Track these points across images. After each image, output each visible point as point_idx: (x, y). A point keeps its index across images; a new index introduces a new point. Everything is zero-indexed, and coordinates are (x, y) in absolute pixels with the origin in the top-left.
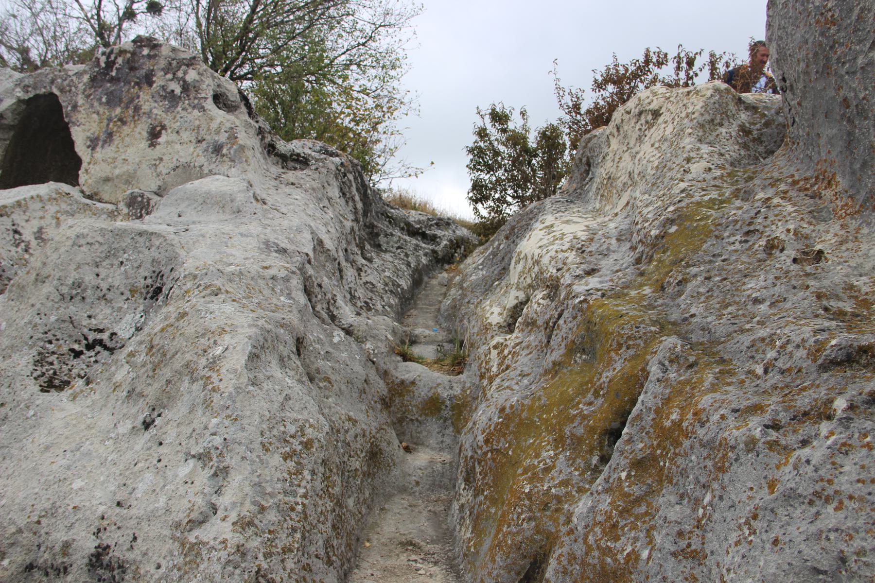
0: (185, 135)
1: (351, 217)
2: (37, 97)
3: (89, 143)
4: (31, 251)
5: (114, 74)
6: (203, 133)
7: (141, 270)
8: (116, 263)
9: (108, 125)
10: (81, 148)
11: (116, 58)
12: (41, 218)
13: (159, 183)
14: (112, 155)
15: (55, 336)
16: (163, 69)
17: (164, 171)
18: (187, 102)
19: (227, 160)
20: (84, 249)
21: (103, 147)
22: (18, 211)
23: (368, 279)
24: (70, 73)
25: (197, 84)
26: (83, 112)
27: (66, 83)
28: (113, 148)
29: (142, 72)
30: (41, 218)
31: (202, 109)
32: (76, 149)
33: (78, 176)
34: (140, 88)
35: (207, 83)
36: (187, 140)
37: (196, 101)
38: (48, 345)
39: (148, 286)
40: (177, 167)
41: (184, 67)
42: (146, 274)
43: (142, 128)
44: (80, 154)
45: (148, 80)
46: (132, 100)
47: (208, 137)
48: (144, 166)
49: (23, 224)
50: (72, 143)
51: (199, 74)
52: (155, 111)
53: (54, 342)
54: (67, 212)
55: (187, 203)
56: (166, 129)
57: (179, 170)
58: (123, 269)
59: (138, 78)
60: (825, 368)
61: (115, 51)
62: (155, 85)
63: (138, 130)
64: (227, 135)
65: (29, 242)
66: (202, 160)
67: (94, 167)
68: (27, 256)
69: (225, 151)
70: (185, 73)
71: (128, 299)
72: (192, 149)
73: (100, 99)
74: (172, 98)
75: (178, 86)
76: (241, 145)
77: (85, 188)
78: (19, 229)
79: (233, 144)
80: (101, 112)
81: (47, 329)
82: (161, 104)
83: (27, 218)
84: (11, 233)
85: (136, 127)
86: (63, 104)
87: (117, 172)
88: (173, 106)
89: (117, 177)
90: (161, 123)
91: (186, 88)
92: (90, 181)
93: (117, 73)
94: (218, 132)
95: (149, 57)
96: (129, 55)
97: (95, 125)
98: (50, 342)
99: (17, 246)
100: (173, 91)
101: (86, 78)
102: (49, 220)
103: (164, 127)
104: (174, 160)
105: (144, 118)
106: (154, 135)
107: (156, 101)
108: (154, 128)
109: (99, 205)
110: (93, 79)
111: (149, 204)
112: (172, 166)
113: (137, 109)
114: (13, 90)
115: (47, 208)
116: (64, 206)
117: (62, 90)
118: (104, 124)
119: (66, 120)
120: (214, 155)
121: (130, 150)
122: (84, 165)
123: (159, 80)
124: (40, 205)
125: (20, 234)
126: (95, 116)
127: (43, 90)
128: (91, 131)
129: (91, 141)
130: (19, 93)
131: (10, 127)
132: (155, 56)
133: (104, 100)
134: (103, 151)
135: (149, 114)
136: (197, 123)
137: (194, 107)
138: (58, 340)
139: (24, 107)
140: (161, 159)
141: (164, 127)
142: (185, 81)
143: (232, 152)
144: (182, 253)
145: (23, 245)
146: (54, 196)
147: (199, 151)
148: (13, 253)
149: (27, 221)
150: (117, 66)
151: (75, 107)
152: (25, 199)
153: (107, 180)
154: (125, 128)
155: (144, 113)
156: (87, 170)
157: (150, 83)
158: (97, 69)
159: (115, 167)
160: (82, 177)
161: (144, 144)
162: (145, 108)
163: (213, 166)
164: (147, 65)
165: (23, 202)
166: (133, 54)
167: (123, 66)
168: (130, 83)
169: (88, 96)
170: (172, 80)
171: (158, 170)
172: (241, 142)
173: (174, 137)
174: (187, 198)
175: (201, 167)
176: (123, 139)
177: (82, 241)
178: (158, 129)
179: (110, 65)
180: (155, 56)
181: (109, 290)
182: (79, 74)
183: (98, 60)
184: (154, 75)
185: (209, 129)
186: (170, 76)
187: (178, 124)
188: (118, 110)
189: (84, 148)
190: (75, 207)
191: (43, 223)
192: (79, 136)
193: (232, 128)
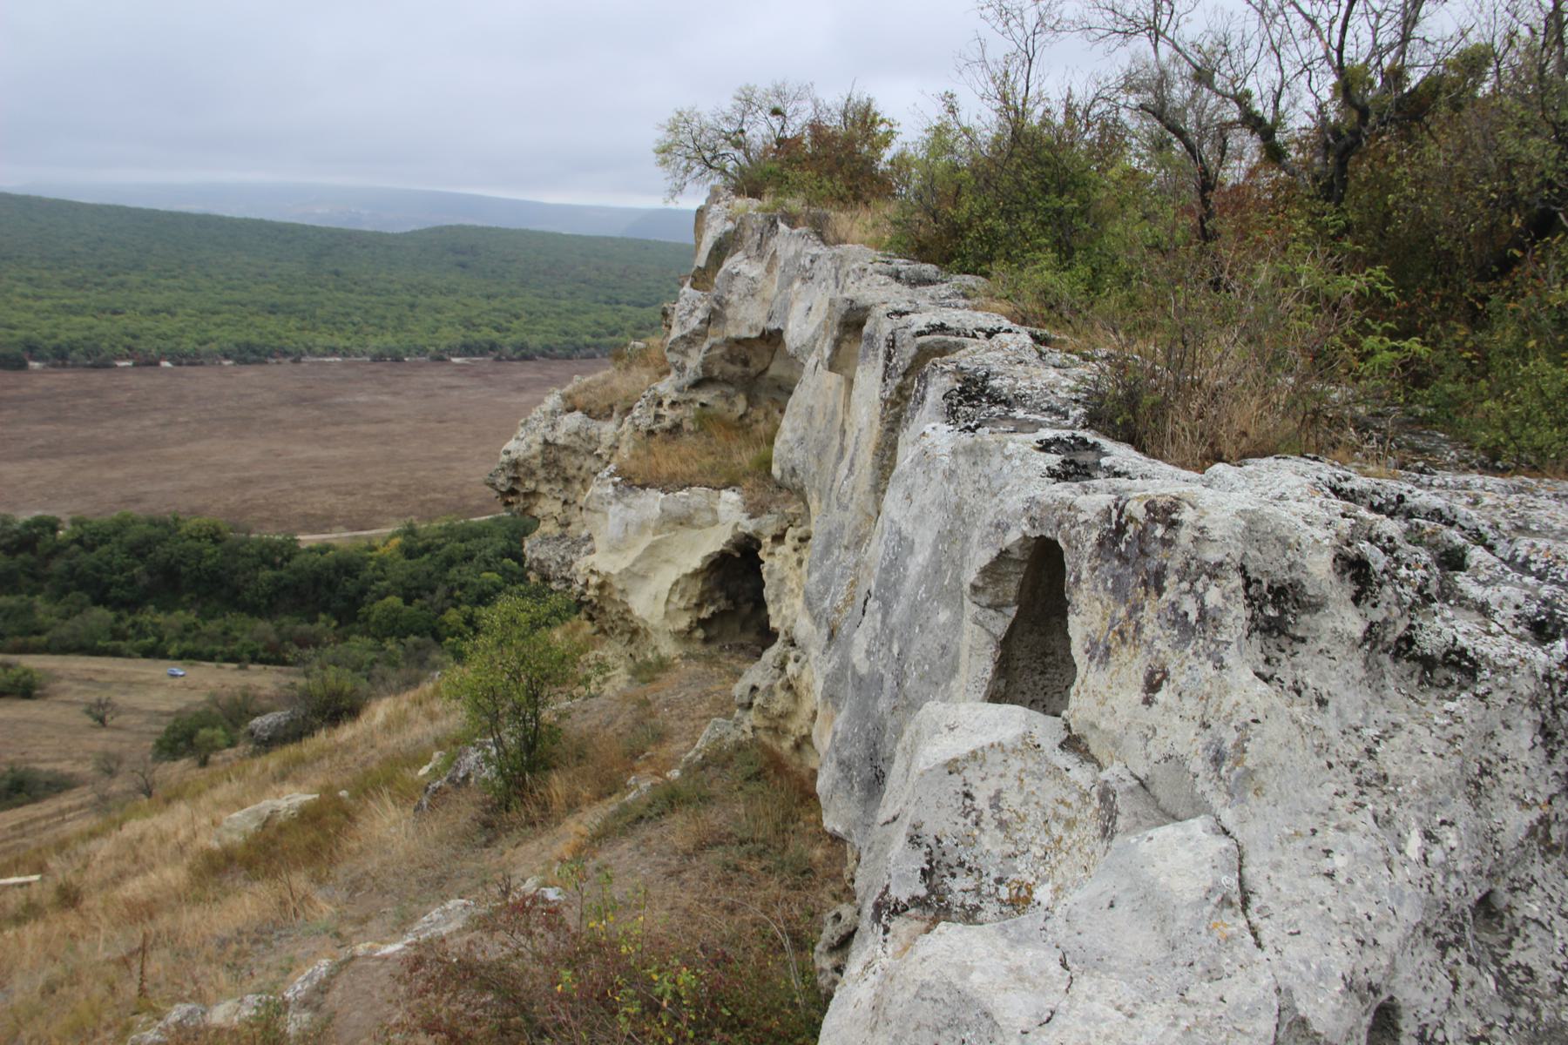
3: (1087, 645)
4: (982, 825)
12: (1001, 776)
16: (1177, 571)
17: (1155, 756)
20: (928, 1004)
22: (972, 765)
23: (1523, 958)
25: (1218, 615)
29: (1152, 565)
30: (1001, 776)
35: (1235, 613)
36: (1189, 713)
41: (1204, 577)
44: (1076, 660)
45: (1156, 581)
48: (1133, 733)
49: (977, 783)
51: (1223, 596)
52: (1158, 644)
54: (1033, 773)
57: (1172, 763)
60: (66, 897)
68: (976, 832)
73: (1105, 581)
76: (1247, 769)
78: (972, 791)
79: (1237, 763)
84: (961, 796)
90: (1163, 666)
99: (966, 816)
100: (1186, 614)
101: (1095, 535)
102: (1011, 781)
106: (1152, 686)
108: (1152, 674)
116: (1030, 764)
124: (1001, 757)
125: (972, 799)
126: (1098, 604)
131: (1018, 562)
133: (1109, 584)
136: (1207, 688)
146: (1020, 746)
147: (1199, 744)
149: (983, 779)
151: (1078, 579)
152: (982, 748)
157: (1160, 590)
162: (1148, 631)
164: (1158, 556)
169: (1094, 569)
177: (926, 994)
178: (1158, 676)
186: (1185, 585)
189: (1081, 652)
190: (1044, 768)
191: (1003, 784)
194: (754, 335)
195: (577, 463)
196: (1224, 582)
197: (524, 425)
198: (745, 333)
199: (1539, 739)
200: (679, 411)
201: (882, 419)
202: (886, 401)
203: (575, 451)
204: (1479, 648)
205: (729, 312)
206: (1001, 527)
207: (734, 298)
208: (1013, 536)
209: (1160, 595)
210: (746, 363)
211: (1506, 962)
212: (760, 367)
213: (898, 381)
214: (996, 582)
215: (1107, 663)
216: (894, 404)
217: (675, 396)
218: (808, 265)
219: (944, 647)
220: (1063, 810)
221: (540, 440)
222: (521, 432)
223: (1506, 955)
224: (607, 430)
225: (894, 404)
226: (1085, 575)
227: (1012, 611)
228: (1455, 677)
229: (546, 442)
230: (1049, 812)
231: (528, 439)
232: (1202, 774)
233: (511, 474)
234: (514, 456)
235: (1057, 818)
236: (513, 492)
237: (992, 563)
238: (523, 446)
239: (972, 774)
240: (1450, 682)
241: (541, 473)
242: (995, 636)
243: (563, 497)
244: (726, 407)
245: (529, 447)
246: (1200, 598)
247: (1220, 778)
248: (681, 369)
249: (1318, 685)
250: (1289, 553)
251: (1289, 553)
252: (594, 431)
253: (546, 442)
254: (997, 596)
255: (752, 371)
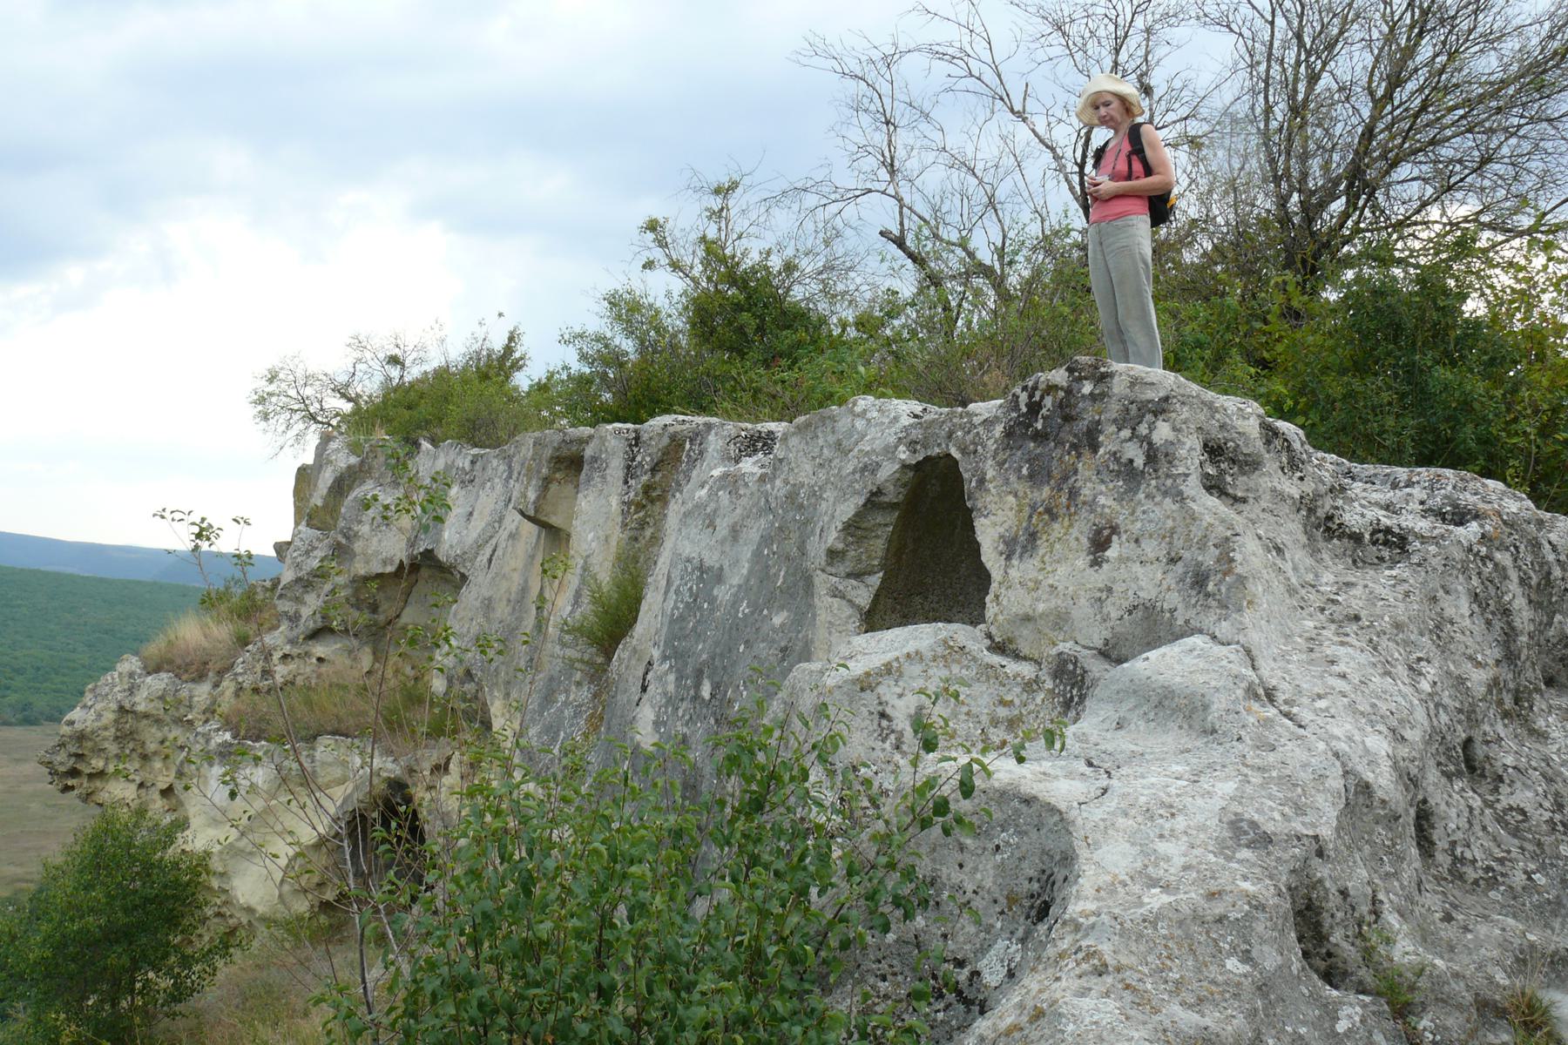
0: (1150, 548)
1: (1493, 653)
2: (927, 459)
3: (1001, 547)
5: (1039, 425)
6: (1179, 543)
7: (1025, 865)
8: (991, 846)
9: (1030, 517)
10: (990, 557)
11: (1042, 398)
13: (1107, 634)
14: (1033, 574)
15: (891, 966)
16: (1115, 421)
17: (1114, 614)
18: (1153, 482)
19: (1214, 604)
21: (1021, 557)
23: (1513, 801)
24: (976, 420)
26: (993, 491)
27: (969, 438)
28: (1036, 562)
29: (1082, 426)
31: (1180, 498)
32: (983, 559)
33: (983, 606)
34: (1079, 456)
36: (1152, 555)
37: (1169, 482)
38: (881, 984)
39: (1032, 896)
40: (1135, 607)
41: (1149, 417)
42: (1032, 873)
43: (1080, 532)
44: (988, 565)
45: (1091, 440)
46: (1065, 478)
47: (1187, 555)
50: (976, 549)
51: (1174, 429)
52: (1102, 500)
53: (889, 977)
55: (1132, 702)
56: (1119, 534)
57: (1139, 614)
58: (998, 857)
59: (1075, 436)
61: (1042, 386)
62: (1102, 451)
63: (1074, 532)
64: (1217, 552)
65: (901, 734)
66: (1173, 599)
67: (1013, 589)
69: (1211, 587)
70: (1152, 428)
71: (1002, 913)
72: (1159, 576)
74: (1130, 474)
75: (1140, 452)
77: (993, 630)
78: (889, 711)
79: (1225, 574)
80: (1021, 494)
81: (880, 956)
82: (1111, 486)
83: (899, 690)
84: (876, 717)
85: (1071, 525)
86: (966, 476)
87: (1041, 607)
88: (1131, 490)
89: (1041, 616)
91: (1152, 457)
92: (1000, 618)
93: (1044, 427)
94: (1202, 546)
95: (1093, 397)
96: (1061, 394)
97: (1011, 514)
98: (884, 979)
100: (1131, 461)
101: (999, 429)
103: (1114, 530)
104: (1130, 593)
105: (1084, 513)
106: (1099, 544)
107: (1102, 481)
108: (1099, 532)
109: (1012, 667)
110: (1009, 433)
111: (1083, 680)
112: (1126, 604)
113: (1073, 494)
114: (896, 447)
115: (931, 672)
117: (963, 451)
118: (1026, 514)
119: (969, 504)
120: (1194, 593)
121: (1062, 570)
122: (994, 586)
123: (1110, 440)
125: (890, 719)
126: (1011, 499)
127: (937, 450)
128: (1006, 526)
129: (1005, 542)
130: (903, 454)
131: (893, 506)
132: (1103, 395)
133: (1025, 471)
134: (1022, 567)
135: (1092, 504)
136: (1170, 523)
137: (1165, 494)
138: (895, 974)
139: (911, 474)
140: (1110, 590)
141: (1114, 530)
142: (1150, 444)
143: (1223, 590)
144: (1083, 853)
145: (893, 737)
147: (1170, 580)
148: (878, 753)
149: (900, 696)
150: (1044, 411)
151: (982, 481)
152: (897, 659)
153: (1027, 619)
154: (1056, 526)
155: (1084, 503)
156: (997, 597)
157: (1094, 448)
158: (1014, 415)
159: (1038, 600)
160: (991, 610)
161: (1082, 561)
162: (1086, 492)
163: (1191, 613)
164: (1089, 414)
165: (895, 664)
166: (1069, 391)
167: (1054, 412)
168: (1063, 444)
169: (1001, 464)
170: (1130, 439)
171: (1105, 611)
172: (1239, 570)
173: (1130, 549)
174: (1135, 692)
175: (1172, 611)
176: (1052, 546)
178: (1106, 533)
179: (1034, 408)
180: (1103, 395)
181: (975, 892)
182: (988, 423)
183: (1016, 397)
184: (1101, 432)
185: (1188, 539)
186: (1126, 433)
187: (1139, 525)
188: (1046, 491)
189: (994, 555)
192: (988, 534)
193: (1227, 539)
194: (390, 569)
195: (159, 735)
196: (1173, 415)
197: (93, 690)
198: (377, 568)
199: (1475, 606)
200: (292, 666)
201: (624, 525)
202: (628, 504)
203: (158, 721)
204: (1404, 525)
205: (358, 546)
206: (870, 469)
207: (365, 529)
208: (888, 470)
209: (1095, 451)
210: (374, 608)
211: (1499, 806)
212: (392, 613)
213: (645, 478)
214: (860, 541)
215: (1034, 548)
216: (640, 506)
217: (287, 649)
218: (467, 466)
219: (784, 650)
220: (1002, 712)
221: (114, 706)
222: (88, 699)
223: (1498, 801)
224: (202, 692)
225: (640, 506)
226: (990, 474)
227: (875, 580)
228: (1386, 553)
229: (121, 709)
230: (985, 719)
231: (98, 706)
232: (1180, 606)
233: (73, 750)
234: (78, 726)
235: (995, 722)
236: (74, 773)
237: (856, 515)
238: (92, 715)
239: (887, 690)
240: (1381, 559)
241: (113, 749)
242: (859, 608)
243: (138, 780)
244: (348, 662)
245: (99, 716)
246: (1147, 440)
247: (1208, 595)
248: (294, 619)
249: (1271, 535)
250: (1217, 416)
251: (1217, 416)
252: (184, 694)
253: (121, 709)
254: (860, 560)
255: (381, 618)
